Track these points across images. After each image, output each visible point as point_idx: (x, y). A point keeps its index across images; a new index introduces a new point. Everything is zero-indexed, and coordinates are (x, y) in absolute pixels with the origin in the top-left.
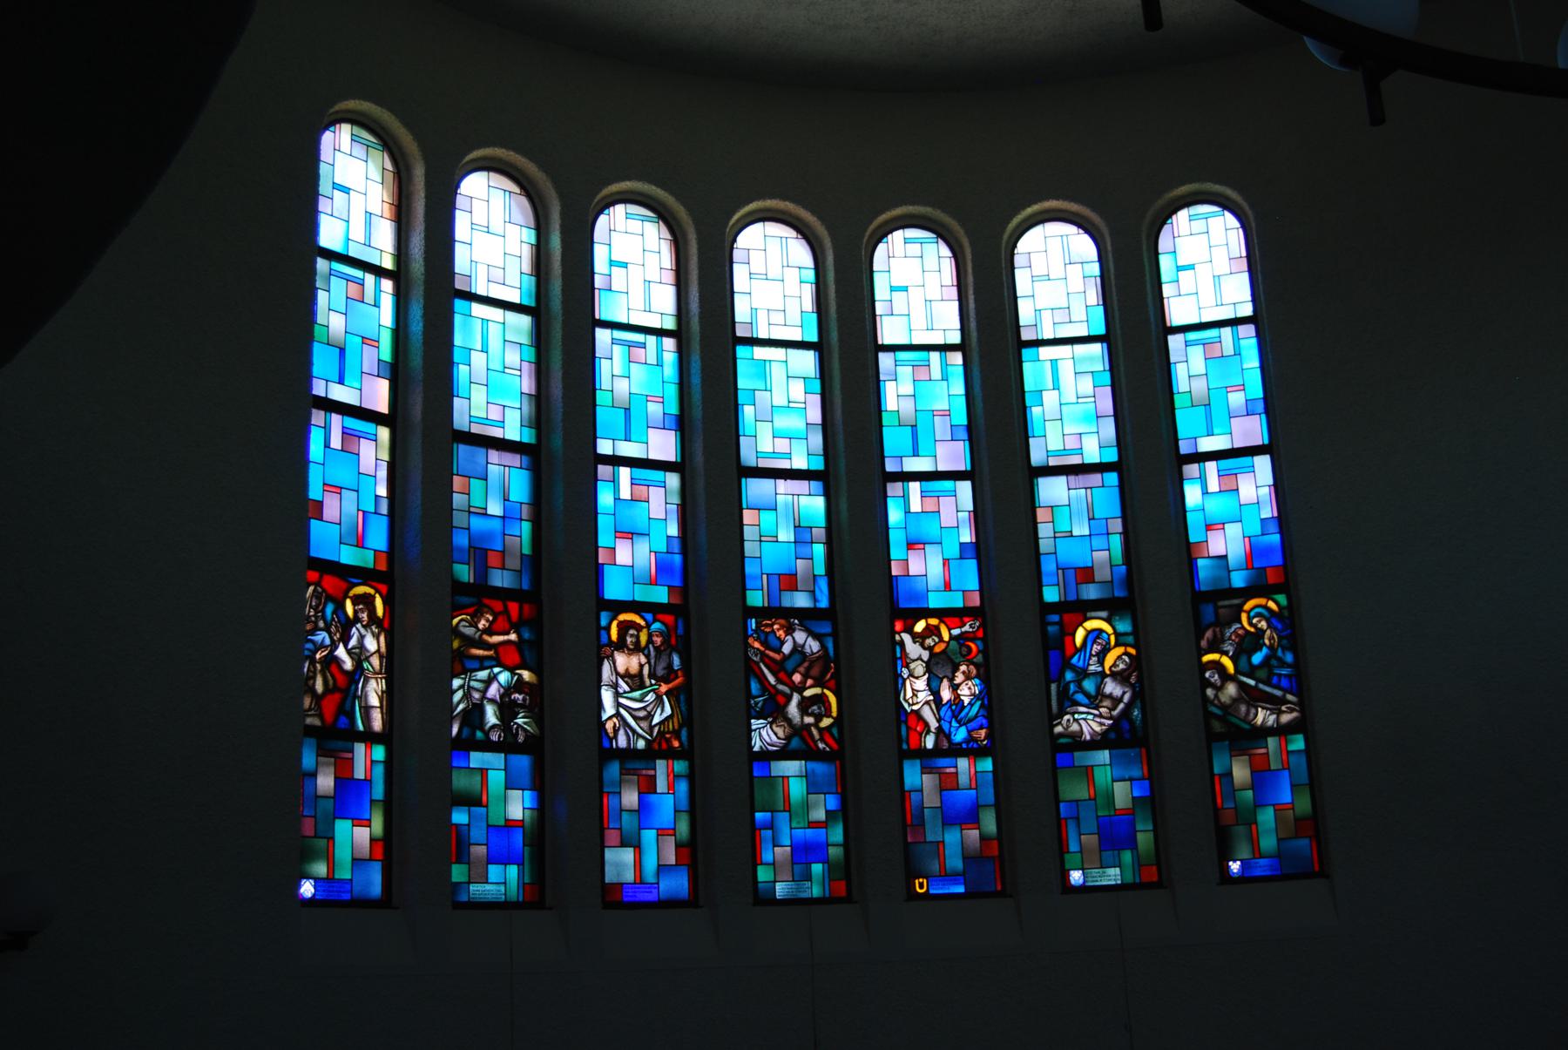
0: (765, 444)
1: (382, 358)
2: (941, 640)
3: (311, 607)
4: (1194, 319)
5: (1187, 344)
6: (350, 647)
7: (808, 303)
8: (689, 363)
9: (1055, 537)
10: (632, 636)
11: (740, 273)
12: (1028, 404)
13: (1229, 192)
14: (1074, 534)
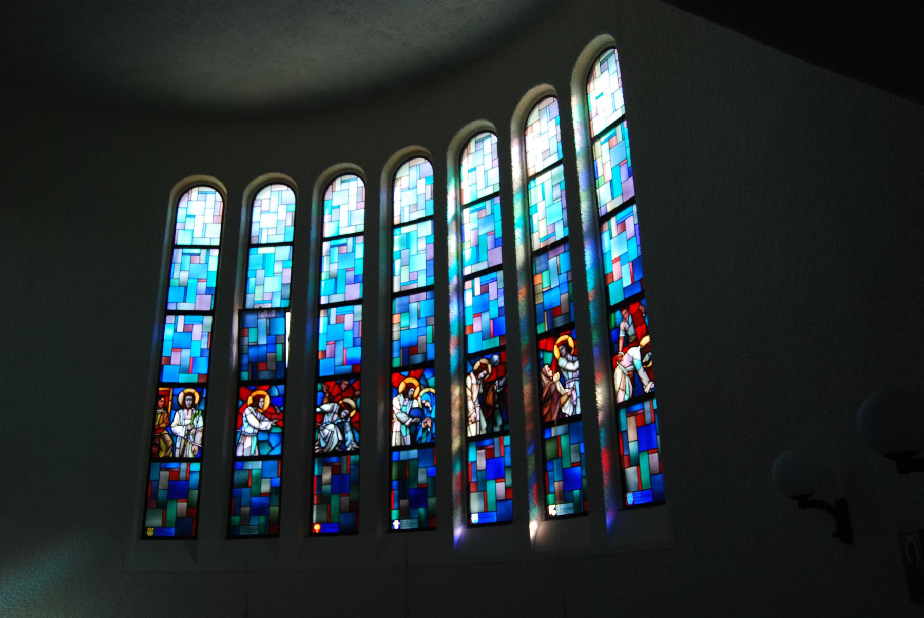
1: (210, 269)
2: (488, 373)
4: (189, 243)
5: (183, 254)
6: (644, 361)
8: (246, 230)
9: (401, 330)
12: (249, 276)
13: (220, 184)
14: (411, 327)
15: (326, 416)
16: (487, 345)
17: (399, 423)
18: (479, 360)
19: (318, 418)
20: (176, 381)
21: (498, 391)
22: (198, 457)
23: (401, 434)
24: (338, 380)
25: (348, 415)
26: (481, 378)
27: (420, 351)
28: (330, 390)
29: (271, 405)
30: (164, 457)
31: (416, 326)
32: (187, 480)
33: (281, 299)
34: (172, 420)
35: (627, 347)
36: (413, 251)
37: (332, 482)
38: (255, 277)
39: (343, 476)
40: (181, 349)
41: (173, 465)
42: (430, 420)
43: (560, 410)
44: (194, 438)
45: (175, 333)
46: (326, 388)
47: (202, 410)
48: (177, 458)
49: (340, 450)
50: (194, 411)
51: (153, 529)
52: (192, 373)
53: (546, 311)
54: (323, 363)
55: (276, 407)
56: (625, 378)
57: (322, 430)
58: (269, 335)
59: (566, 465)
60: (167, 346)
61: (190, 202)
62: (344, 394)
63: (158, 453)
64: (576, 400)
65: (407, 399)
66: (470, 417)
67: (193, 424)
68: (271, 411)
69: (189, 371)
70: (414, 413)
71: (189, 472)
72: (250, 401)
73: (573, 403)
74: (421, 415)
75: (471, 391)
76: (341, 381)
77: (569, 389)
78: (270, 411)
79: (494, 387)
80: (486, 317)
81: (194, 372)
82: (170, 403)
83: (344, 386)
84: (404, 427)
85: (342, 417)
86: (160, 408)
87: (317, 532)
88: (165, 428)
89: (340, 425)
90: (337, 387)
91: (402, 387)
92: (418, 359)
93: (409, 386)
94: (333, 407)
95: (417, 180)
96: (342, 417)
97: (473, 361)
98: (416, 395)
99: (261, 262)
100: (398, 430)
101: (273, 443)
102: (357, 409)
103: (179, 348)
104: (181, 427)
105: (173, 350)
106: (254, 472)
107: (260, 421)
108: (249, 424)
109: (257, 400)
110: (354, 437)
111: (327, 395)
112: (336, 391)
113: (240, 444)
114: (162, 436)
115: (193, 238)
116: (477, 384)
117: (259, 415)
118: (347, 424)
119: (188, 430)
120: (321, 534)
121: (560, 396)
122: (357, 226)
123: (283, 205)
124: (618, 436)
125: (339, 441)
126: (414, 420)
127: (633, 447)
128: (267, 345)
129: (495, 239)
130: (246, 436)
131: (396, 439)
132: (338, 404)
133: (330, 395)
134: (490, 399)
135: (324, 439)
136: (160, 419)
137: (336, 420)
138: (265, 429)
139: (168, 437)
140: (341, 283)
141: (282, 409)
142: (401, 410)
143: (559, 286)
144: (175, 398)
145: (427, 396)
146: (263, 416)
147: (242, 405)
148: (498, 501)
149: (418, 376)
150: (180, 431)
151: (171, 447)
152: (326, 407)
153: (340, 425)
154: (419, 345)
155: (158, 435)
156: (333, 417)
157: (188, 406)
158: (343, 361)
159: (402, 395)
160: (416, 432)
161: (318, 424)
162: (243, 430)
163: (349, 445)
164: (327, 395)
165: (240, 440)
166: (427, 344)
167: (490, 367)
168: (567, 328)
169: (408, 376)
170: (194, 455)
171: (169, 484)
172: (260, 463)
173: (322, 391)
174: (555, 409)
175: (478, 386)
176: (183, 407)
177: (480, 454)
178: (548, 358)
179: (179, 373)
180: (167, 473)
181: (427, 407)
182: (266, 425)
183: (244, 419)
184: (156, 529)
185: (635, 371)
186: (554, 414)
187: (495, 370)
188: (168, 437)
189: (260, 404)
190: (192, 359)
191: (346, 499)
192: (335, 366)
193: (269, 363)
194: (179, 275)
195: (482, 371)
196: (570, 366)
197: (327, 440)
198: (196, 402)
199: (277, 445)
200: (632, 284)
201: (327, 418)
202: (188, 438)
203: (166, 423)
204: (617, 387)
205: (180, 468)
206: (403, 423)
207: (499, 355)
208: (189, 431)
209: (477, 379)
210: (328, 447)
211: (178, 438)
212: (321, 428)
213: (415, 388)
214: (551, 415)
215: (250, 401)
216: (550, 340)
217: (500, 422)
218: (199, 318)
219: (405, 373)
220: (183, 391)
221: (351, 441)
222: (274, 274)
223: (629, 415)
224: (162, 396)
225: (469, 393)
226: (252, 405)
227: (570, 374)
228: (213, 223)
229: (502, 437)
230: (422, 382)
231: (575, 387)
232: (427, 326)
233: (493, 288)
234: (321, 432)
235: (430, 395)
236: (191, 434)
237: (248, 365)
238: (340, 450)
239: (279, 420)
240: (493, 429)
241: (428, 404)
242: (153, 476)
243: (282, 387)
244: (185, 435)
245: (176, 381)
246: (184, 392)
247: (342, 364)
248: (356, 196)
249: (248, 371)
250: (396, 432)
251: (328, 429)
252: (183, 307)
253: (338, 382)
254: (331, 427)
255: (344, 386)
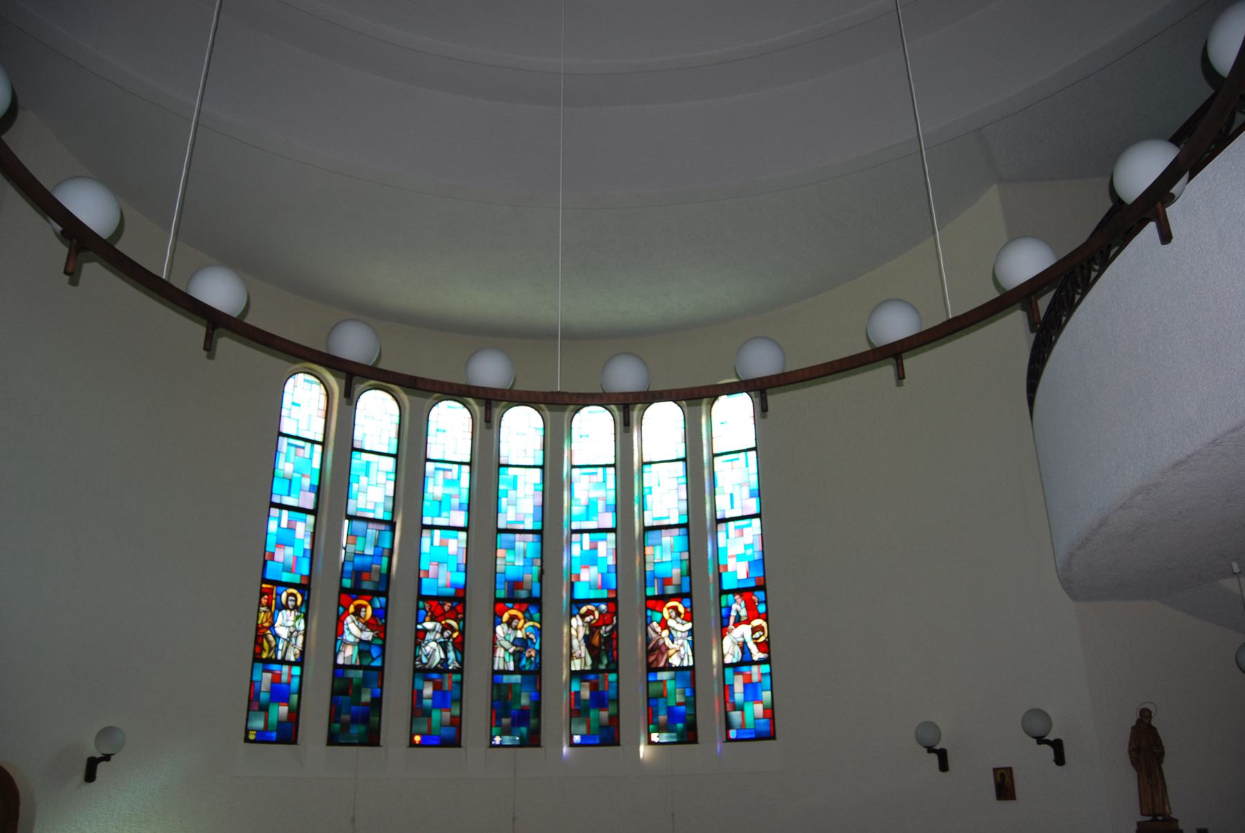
1: (313, 466)
2: (594, 618)
4: (294, 434)
9: (506, 565)
15: (428, 634)
16: (593, 595)
17: (502, 650)
19: (421, 634)
20: (278, 579)
22: (299, 660)
23: (505, 660)
25: (450, 636)
26: (587, 622)
27: (525, 586)
28: (432, 609)
29: (373, 616)
31: (522, 564)
32: (289, 683)
37: (433, 697)
41: (275, 667)
43: (667, 660)
44: (296, 641)
48: (279, 661)
50: (297, 613)
53: (657, 578)
54: (425, 581)
57: (424, 647)
58: (376, 546)
59: (671, 703)
60: (271, 540)
68: (373, 622)
69: (291, 570)
70: (517, 642)
71: (291, 676)
72: (352, 609)
73: (680, 657)
74: (525, 645)
75: (577, 631)
78: (373, 622)
79: (600, 632)
82: (274, 602)
83: (446, 608)
84: (507, 654)
86: (263, 606)
87: (417, 743)
88: (268, 628)
89: (443, 644)
90: (439, 607)
91: (506, 617)
92: (523, 594)
93: (513, 617)
94: (435, 626)
96: (445, 636)
97: (580, 605)
98: (520, 626)
100: (502, 655)
101: (375, 654)
104: (284, 628)
106: (355, 681)
107: (361, 630)
108: (351, 633)
109: (358, 609)
111: (429, 614)
112: (438, 611)
114: (265, 636)
116: (583, 626)
117: (361, 625)
118: (450, 644)
120: (421, 745)
121: (668, 649)
124: (727, 690)
125: (441, 659)
130: (348, 644)
132: (441, 624)
133: (432, 613)
134: (596, 640)
135: (426, 656)
138: (366, 639)
139: (271, 638)
141: (383, 621)
142: (505, 638)
143: (671, 561)
144: (278, 597)
145: (532, 629)
146: (364, 627)
148: (602, 727)
149: (523, 609)
150: (283, 632)
152: (429, 625)
156: (435, 635)
157: (291, 607)
162: (344, 638)
164: (429, 614)
166: (532, 582)
167: (597, 614)
168: (679, 596)
169: (512, 608)
172: (361, 672)
174: (662, 659)
176: (286, 607)
177: (584, 686)
180: (269, 675)
181: (531, 639)
182: (368, 635)
183: (345, 626)
184: (259, 732)
185: (745, 643)
186: (661, 662)
188: (271, 638)
189: (362, 614)
193: (373, 574)
194: (285, 466)
199: (378, 657)
201: (429, 636)
202: (291, 640)
203: (270, 622)
205: (281, 671)
206: (506, 650)
208: (292, 633)
209: (583, 621)
210: (430, 663)
211: (281, 639)
212: (423, 645)
213: (519, 620)
214: (657, 662)
215: (352, 609)
217: (605, 661)
218: (303, 515)
219: (510, 605)
220: (285, 590)
223: (737, 673)
225: (574, 632)
226: (353, 614)
227: (679, 634)
229: (606, 674)
230: (527, 615)
232: (532, 565)
234: (423, 649)
235: (535, 629)
237: (352, 573)
239: (381, 632)
240: (597, 666)
241: (532, 636)
242: (256, 678)
243: (383, 600)
244: (288, 637)
249: (351, 578)
253: (441, 602)
254: (433, 645)
255: (446, 608)
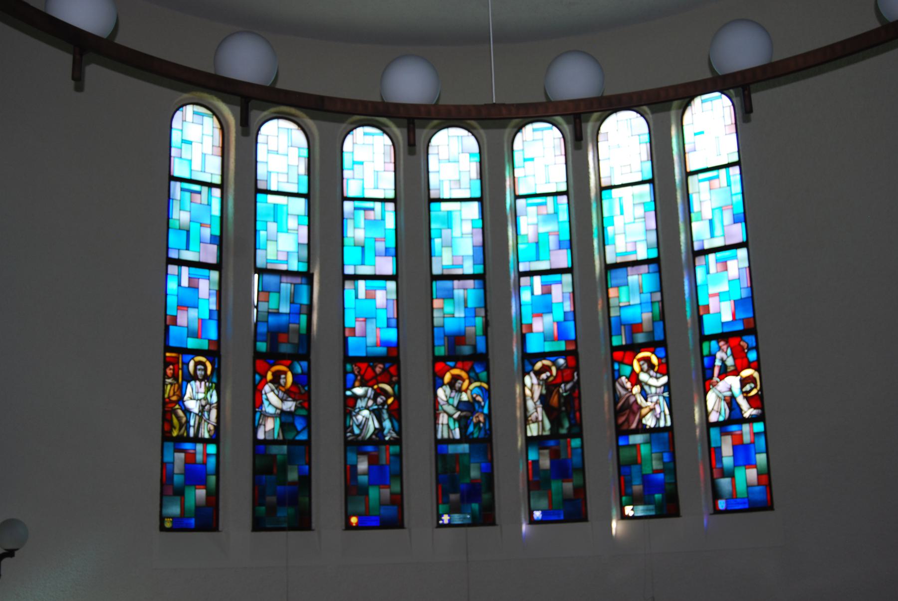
0: (271, 256)
2: (551, 375)
3: (353, 372)
4: (186, 175)
6: (744, 390)
7: (303, 169)
10: (459, 383)
11: (261, 149)
15: (359, 401)
16: (548, 347)
17: (446, 416)
18: (541, 360)
21: (565, 394)
22: (214, 437)
24: (372, 362)
25: (385, 402)
26: (543, 380)
27: (468, 341)
28: (362, 372)
30: (178, 436)
32: (205, 463)
33: (299, 261)
34: (184, 393)
35: (724, 375)
36: (456, 232)
37: (369, 472)
38: (266, 230)
39: (382, 467)
40: (188, 307)
41: (188, 446)
42: (482, 415)
43: (640, 420)
45: (180, 288)
46: (358, 370)
47: (215, 383)
48: (192, 438)
49: (378, 439)
50: (207, 384)
51: (171, 520)
52: (201, 338)
54: (351, 340)
55: (300, 386)
56: (720, 402)
57: (355, 416)
58: (292, 303)
59: (647, 470)
61: (184, 123)
62: (379, 378)
63: (171, 432)
64: (660, 414)
65: (454, 391)
66: (530, 416)
67: (207, 398)
69: (197, 335)
71: (206, 455)
72: (269, 376)
73: (656, 416)
76: (375, 364)
77: (652, 402)
78: (293, 390)
79: (558, 391)
80: (548, 319)
81: (203, 337)
83: (378, 370)
85: (378, 403)
86: (169, 378)
88: (177, 402)
89: (376, 412)
90: (370, 369)
91: (447, 378)
92: (466, 350)
93: (455, 378)
94: (367, 392)
95: (459, 153)
96: (378, 403)
97: (533, 360)
99: (272, 213)
100: (445, 422)
101: (299, 427)
102: (394, 395)
103: (185, 307)
105: (179, 308)
107: (282, 400)
108: (270, 404)
110: (393, 426)
111: (359, 378)
113: (261, 425)
114: (174, 411)
115: (191, 170)
117: (281, 394)
118: (385, 411)
119: (202, 406)
121: (640, 408)
122: (204, 133)
123: (293, 147)
124: (714, 453)
125: (376, 429)
126: (464, 413)
127: (728, 460)
128: (289, 314)
129: (560, 242)
130: (268, 417)
131: (442, 432)
132: (373, 389)
134: (555, 400)
135: (358, 426)
136: (170, 390)
137: (372, 406)
138: (289, 410)
139: (180, 413)
140: (369, 254)
141: (306, 388)
142: (447, 401)
144: (185, 367)
145: (478, 391)
146: (285, 395)
147: (260, 381)
151: (185, 425)
152: (359, 391)
153: (376, 412)
154: (467, 335)
155: (170, 409)
158: (377, 343)
159: (448, 387)
160: (467, 427)
161: (349, 409)
162: (263, 409)
163: (387, 434)
164: (359, 378)
165: (261, 421)
168: (651, 345)
169: (455, 367)
170: (210, 435)
171: (186, 468)
172: (285, 448)
173: (353, 372)
175: (540, 387)
176: (195, 378)
178: (626, 370)
179: (188, 337)
180: (182, 455)
181: (479, 402)
182: (290, 405)
183: (264, 396)
184: (175, 519)
185: (733, 397)
187: (560, 374)
188: (180, 413)
189: (282, 381)
190: (200, 321)
191: (386, 492)
192: (367, 347)
194: (180, 215)
195: (545, 372)
196: (653, 382)
197: (361, 427)
198: (209, 372)
199: (304, 429)
200: (733, 321)
201: (360, 404)
202: (203, 415)
203: (178, 395)
204: (710, 408)
205: (195, 450)
206: (450, 416)
207: (565, 359)
209: (538, 379)
210: (362, 435)
211: (192, 414)
212: (354, 413)
213: (464, 380)
214: (629, 423)
215: (269, 376)
216: (628, 354)
217: (566, 424)
219: (451, 364)
221: (390, 430)
222: (288, 231)
224: (171, 364)
225: (528, 392)
226: (271, 381)
227: (653, 390)
228: (212, 155)
230: (472, 374)
231: (658, 402)
232: (475, 316)
233: (557, 292)
234: (354, 418)
235: (482, 391)
236: (205, 410)
238: (378, 439)
240: (558, 430)
241: (479, 399)
243: (304, 364)
244: (200, 411)
245: (185, 346)
246: (194, 360)
247: (375, 345)
248: (383, 155)
250: (442, 424)
251: (361, 415)
252: (187, 256)
253: (371, 364)
254: (366, 413)
255: (378, 370)
